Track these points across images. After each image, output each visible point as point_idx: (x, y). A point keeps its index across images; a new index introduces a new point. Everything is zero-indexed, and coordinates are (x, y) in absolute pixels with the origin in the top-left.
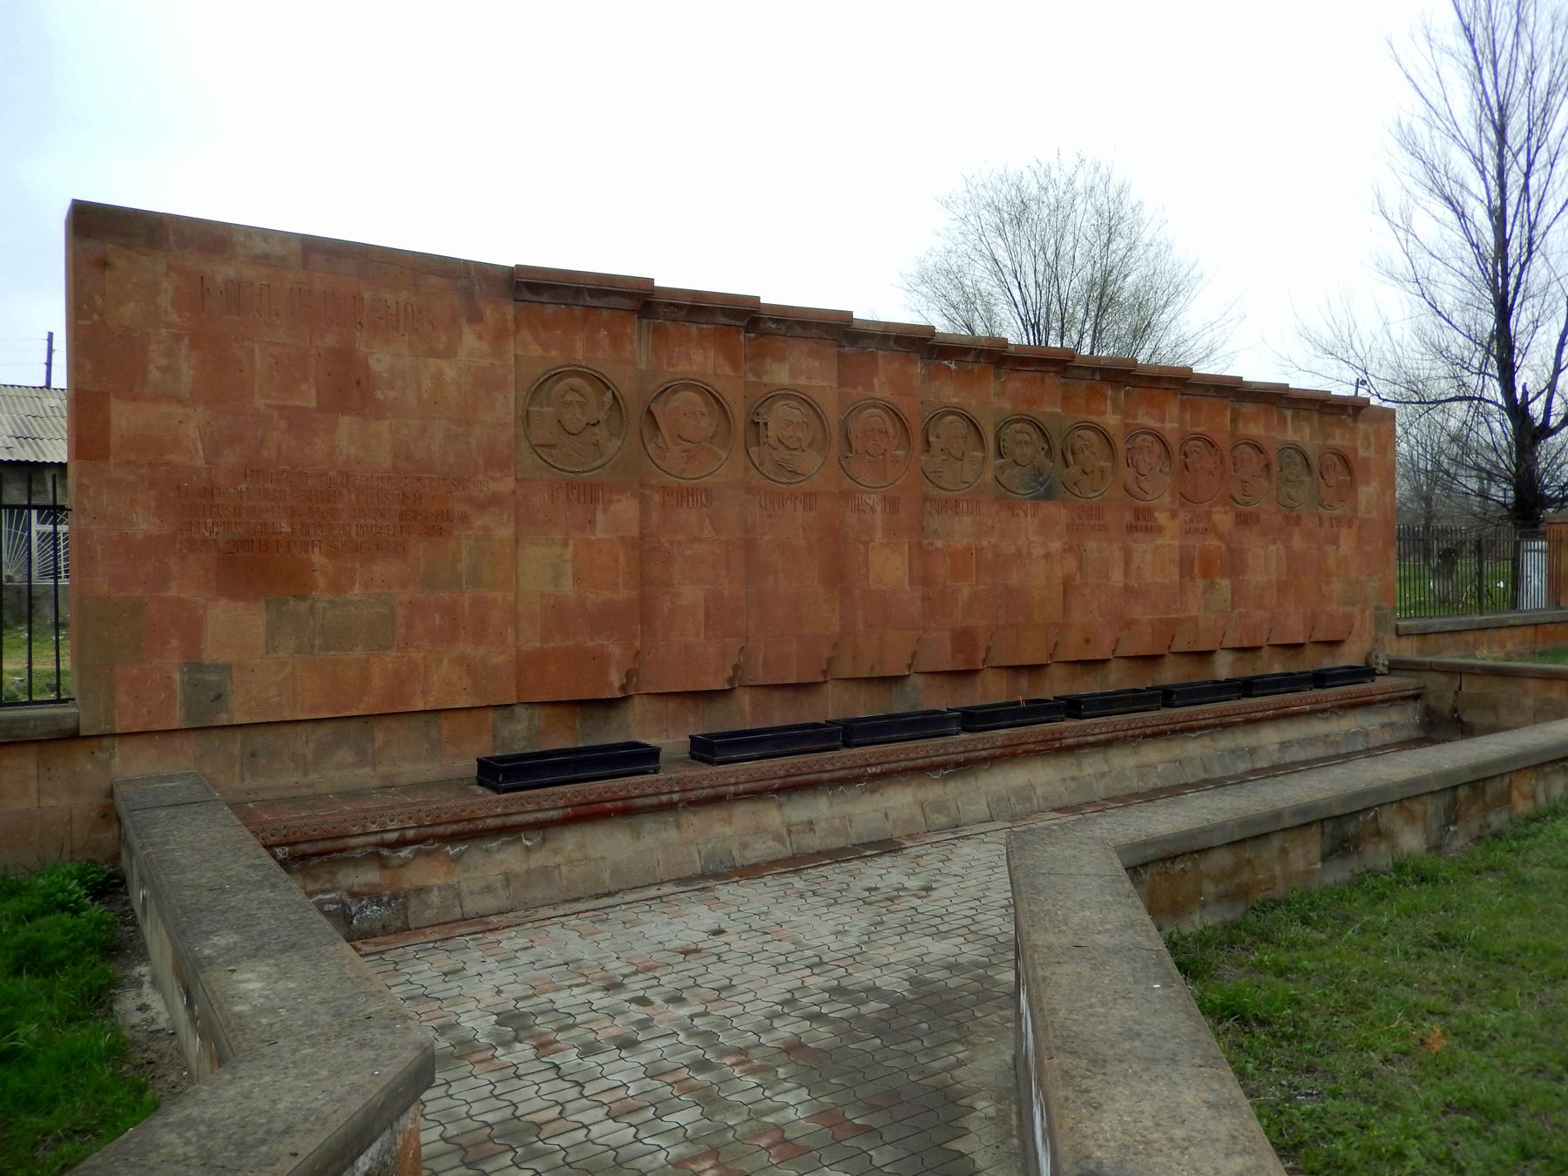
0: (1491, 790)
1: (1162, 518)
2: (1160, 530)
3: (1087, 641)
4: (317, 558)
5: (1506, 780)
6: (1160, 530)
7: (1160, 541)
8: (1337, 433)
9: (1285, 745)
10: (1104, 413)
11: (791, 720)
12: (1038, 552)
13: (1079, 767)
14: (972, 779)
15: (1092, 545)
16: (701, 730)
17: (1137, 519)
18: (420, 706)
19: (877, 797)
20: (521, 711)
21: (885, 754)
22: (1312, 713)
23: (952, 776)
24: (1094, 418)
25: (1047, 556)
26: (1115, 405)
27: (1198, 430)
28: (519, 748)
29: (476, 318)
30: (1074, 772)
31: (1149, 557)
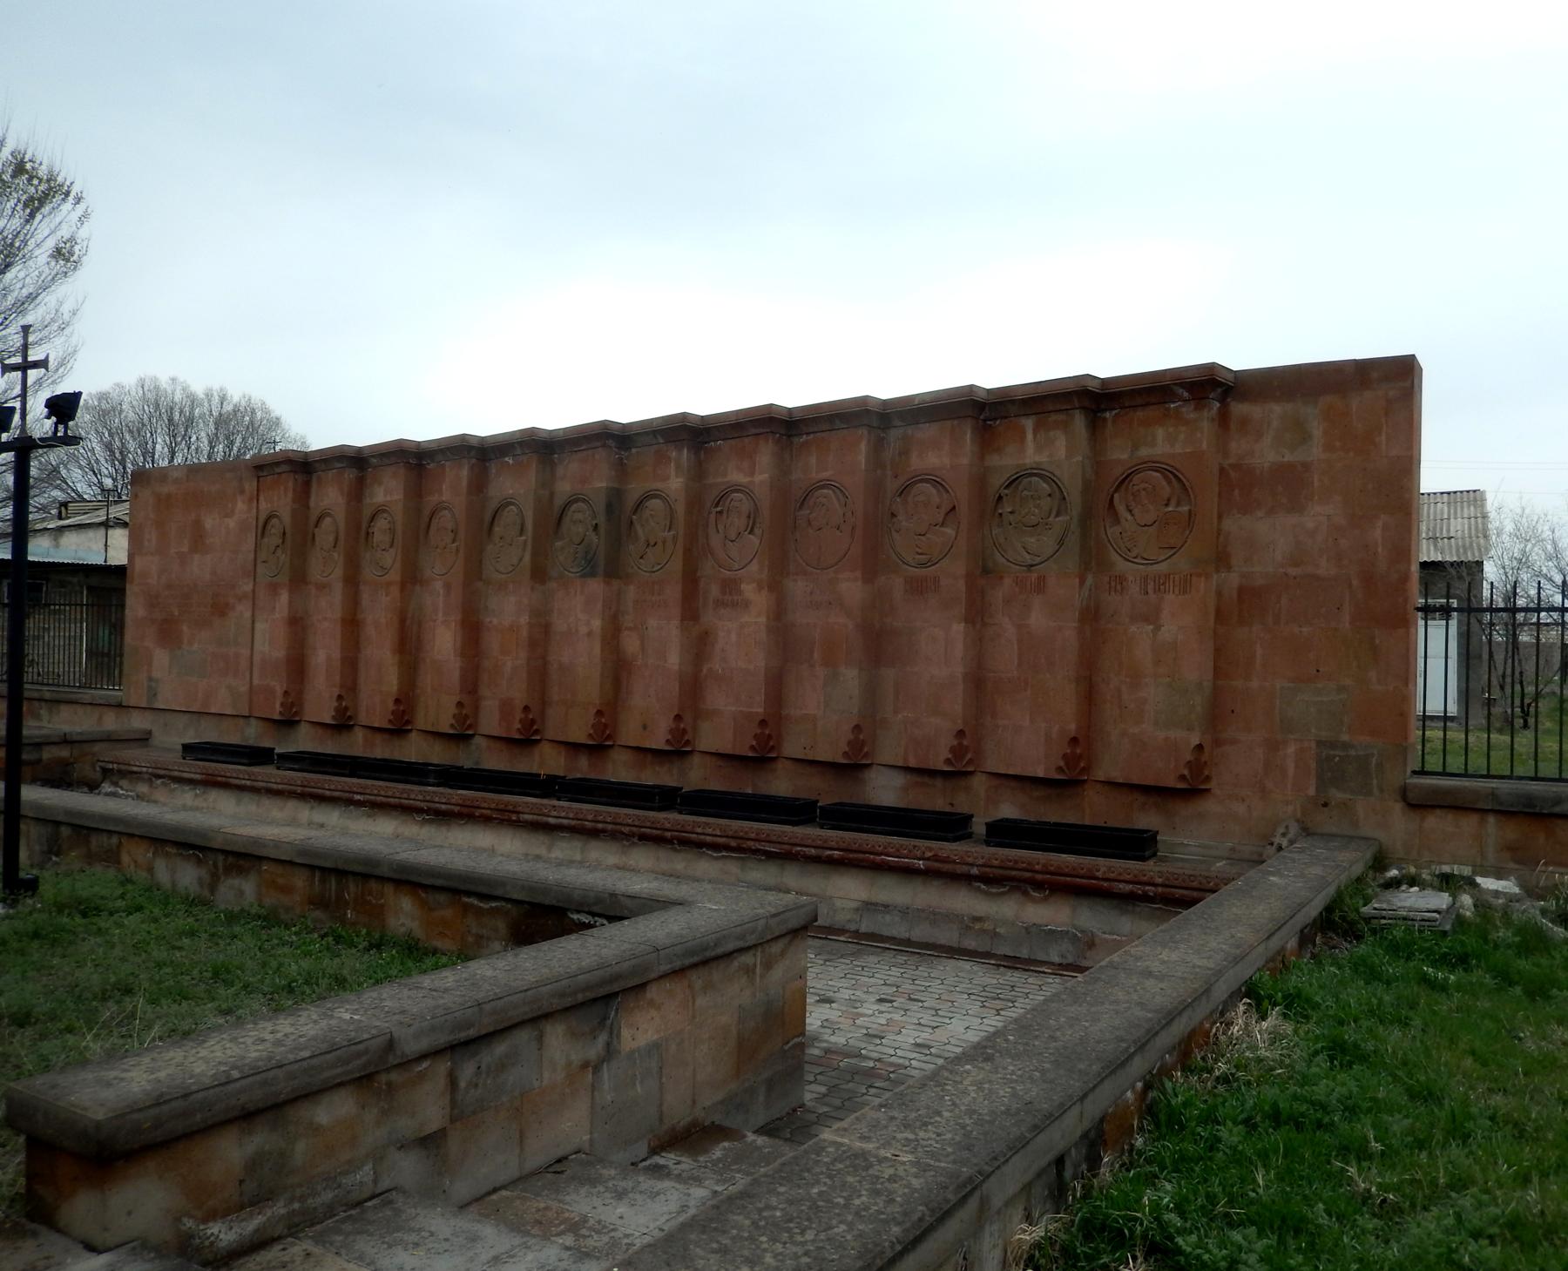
0: (96, 842)
1: (748, 590)
2: (746, 604)
3: (645, 727)
4: (185, 628)
5: (115, 840)
6: (746, 604)
7: (746, 619)
8: (1160, 433)
9: (869, 907)
10: (668, 478)
11: (387, 756)
12: (583, 630)
13: (549, 849)
14: (444, 829)
15: (652, 623)
16: (190, 738)
17: (724, 593)
18: (213, 710)
19: (370, 821)
20: (253, 721)
21: (366, 787)
22: (928, 874)
23: (430, 822)
24: (659, 485)
25: (590, 634)
26: (678, 467)
27: (825, 475)
28: (251, 742)
29: (242, 492)
30: (542, 851)
31: (734, 637)
